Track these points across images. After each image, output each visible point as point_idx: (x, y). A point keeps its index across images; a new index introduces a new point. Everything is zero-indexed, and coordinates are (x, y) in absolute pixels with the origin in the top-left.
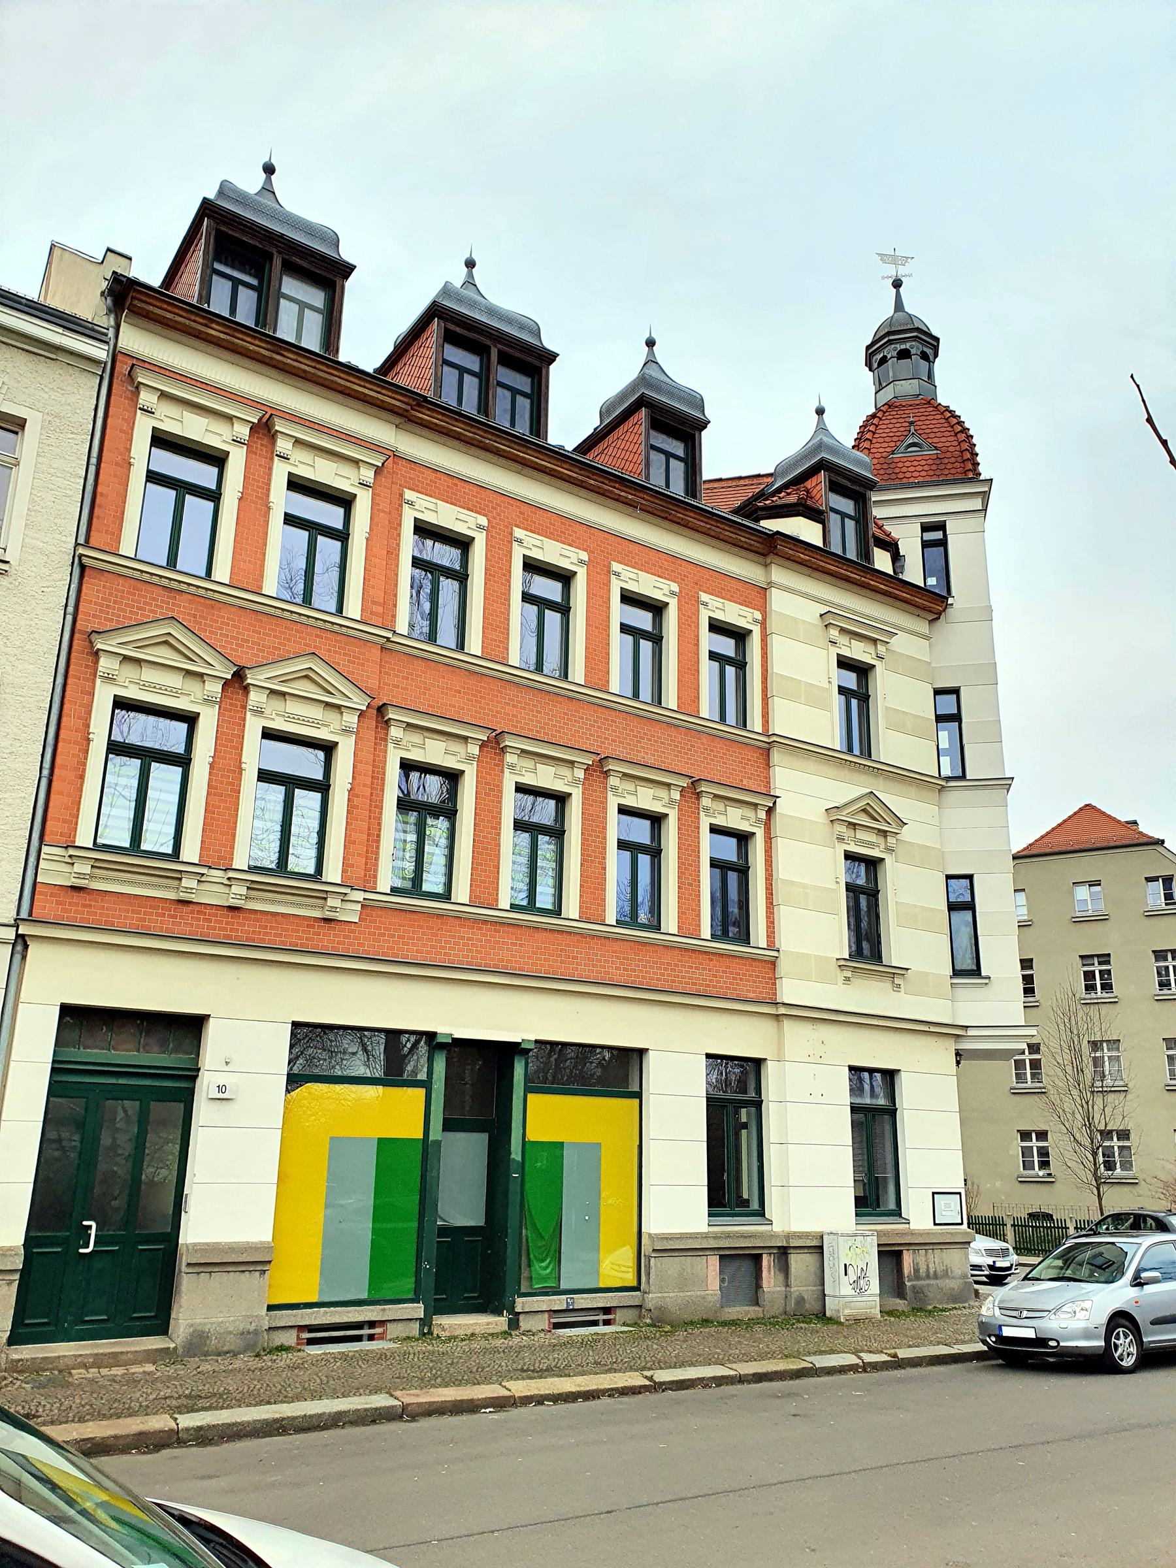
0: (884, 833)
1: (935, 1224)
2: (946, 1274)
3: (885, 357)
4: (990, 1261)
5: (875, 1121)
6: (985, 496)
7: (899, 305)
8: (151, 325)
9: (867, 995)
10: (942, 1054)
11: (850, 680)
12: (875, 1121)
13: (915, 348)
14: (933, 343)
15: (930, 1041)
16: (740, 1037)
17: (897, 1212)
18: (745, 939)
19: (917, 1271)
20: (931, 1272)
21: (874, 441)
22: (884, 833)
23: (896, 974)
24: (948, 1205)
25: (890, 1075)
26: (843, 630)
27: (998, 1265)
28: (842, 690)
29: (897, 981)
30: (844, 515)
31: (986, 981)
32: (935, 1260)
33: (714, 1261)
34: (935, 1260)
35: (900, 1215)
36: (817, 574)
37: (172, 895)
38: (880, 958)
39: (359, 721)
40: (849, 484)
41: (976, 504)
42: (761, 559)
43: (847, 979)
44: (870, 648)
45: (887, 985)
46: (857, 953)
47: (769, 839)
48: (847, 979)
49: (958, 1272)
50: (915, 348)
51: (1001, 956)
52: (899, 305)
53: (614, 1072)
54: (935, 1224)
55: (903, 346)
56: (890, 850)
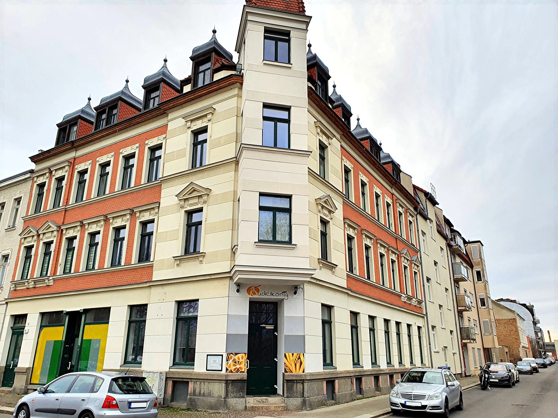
0: (330, 212)
1: (207, 370)
2: (210, 395)
4: (403, 401)
5: (186, 321)
8: (91, 143)
9: (323, 274)
10: (224, 288)
12: (186, 321)
15: (216, 283)
16: (137, 297)
17: (331, 364)
19: (194, 391)
20: (202, 392)
22: (330, 212)
23: (332, 267)
24: (215, 361)
26: (321, 130)
27: (408, 404)
29: (201, 259)
32: (205, 388)
33: (325, 383)
34: (205, 388)
35: (359, 364)
36: (184, 105)
37: (45, 285)
39: (235, 173)
40: (203, 58)
43: (178, 265)
48: (178, 265)
49: (216, 395)
51: (338, 256)
53: (102, 315)
54: (207, 370)
56: (205, 202)
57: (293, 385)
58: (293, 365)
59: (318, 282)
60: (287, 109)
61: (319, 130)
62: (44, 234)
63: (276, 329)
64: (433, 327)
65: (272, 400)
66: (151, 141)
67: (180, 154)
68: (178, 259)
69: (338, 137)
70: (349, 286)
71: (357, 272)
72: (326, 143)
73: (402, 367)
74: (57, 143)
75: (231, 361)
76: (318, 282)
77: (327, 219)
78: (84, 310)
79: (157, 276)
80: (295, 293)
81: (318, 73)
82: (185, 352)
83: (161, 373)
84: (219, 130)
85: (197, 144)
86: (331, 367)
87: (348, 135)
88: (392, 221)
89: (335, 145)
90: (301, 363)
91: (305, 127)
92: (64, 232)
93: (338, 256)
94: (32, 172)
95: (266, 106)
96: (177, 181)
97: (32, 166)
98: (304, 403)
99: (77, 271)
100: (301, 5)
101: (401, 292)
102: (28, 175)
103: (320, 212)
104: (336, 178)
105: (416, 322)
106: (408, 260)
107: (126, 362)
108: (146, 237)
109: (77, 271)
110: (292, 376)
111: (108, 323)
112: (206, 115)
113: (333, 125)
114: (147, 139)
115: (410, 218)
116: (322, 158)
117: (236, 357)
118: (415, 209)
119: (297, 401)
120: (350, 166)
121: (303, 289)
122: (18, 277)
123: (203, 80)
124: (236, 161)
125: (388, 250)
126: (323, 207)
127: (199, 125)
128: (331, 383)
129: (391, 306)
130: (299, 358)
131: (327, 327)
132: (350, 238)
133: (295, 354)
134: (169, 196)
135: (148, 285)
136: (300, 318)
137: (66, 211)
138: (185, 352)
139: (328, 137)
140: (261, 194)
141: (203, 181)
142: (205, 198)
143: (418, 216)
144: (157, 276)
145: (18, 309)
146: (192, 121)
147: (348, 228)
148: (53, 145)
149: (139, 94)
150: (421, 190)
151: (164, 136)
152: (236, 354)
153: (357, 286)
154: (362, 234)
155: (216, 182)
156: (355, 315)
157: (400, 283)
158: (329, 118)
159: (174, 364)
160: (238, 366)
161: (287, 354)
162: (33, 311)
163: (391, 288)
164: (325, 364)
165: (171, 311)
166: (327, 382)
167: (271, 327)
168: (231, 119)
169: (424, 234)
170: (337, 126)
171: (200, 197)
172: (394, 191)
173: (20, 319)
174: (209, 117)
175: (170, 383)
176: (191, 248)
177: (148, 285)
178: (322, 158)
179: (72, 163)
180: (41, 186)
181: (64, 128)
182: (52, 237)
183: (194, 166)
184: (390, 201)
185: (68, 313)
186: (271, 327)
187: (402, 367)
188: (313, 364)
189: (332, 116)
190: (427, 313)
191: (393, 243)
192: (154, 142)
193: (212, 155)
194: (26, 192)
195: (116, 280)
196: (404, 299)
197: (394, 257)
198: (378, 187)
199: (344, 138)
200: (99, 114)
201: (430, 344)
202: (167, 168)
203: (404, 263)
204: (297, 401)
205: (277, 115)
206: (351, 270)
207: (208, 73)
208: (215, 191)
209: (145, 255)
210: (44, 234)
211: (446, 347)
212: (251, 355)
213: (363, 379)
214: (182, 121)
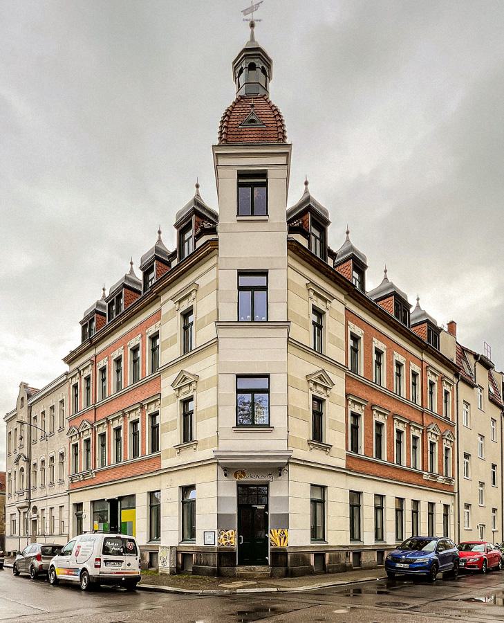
0: (326, 388)
3: (242, 68)
6: (287, 154)
7: (252, 39)
9: (317, 456)
10: (212, 472)
11: (315, 318)
13: (259, 64)
14: (267, 62)
16: (152, 485)
17: (382, 539)
18: (357, 452)
21: (231, 117)
22: (326, 388)
23: (327, 448)
25: (323, 488)
26: (315, 293)
28: (314, 323)
30: (316, 238)
31: (272, 429)
33: (376, 553)
38: (322, 441)
41: (282, 160)
42: (421, 350)
44: (324, 303)
45: (324, 453)
46: (314, 438)
47: (423, 438)
50: (259, 64)
51: (336, 436)
52: (252, 39)
55: (254, 61)
57: (278, 557)
58: (278, 541)
59: (305, 463)
60: (264, 273)
61: (312, 293)
62: (83, 432)
63: (267, 508)
64: (468, 506)
65: (260, 569)
66: (150, 329)
67: (172, 341)
68: (179, 449)
69: (342, 298)
70: (350, 465)
71: (362, 451)
72: (323, 309)
73: (358, 544)
74: (83, 341)
75: (222, 537)
76: (305, 463)
77: (322, 396)
78: (119, 497)
79: (165, 463)
80: (280, 475)
81: (308, 219)
82: (189, 529)
83: (171, 547)
84: (204, 307)
85: (186, 327)
86: (323, 542)
87: (355, 295)
88: (419, 393)
89: (337, 307)
90: (285, 538)
91: (291, 289)
92: (97, 429)
93: (336, 436)
94: (67, 374)
95: (241, 273)
96: (171, 370)
97: (66, 368)
98: (287, 571)
99: (109, 464)
100: (278, 118)
101: (423, 470)
102: (65, 378)
103: (311, 389)
104: (336, 350)
105: (440, 500)
106: (436, 435)
107: (151, 540)
108: (155, 429)
109: (109, 464)
110: (277, 549)
111: (135, 508)
112: (190, 294)
113: (333, 284)
114: (147, 328)
115: (447, 388)
116: (319, 326)
117: (227, 533)
118: (456, 375)
119: (282, 570)
120: (358, 331)
121: (288, 471)
122: (72, 472)
123: (189, 249)
124: (216, 342)
125: (409, 425)
126: (315, 384)
127: (185, 305)
128: (357, 554)
129: (408, 484)
130: (284, 533)
131: (319, 507)
132: (356, 416)
133: (280, 530)
134: (166, 387)
135: (158, 473)
136: (290, 499)
137: (95, 409)
138: (189, 529)
139: (326, 301)
140: (238, 376)
141: (191, 368)
142: (194, 385)
143: (461, 384)
144: (165, 463)
145: (76, 498)
146: (180, 302)
147: (352, 405)
148: (80, 343)
149: (139, 275)
150: (470, 352)
151: (159, 322)
152: (227, 531)
153: (355, 466)
154: (373, 410)
155: (203, 367)
156: (356, 496)
157: (423, 461)
158: (327, 276)
159: (183, 541)
160: (229, 541)
161: (272, 531)
162: (86, 498)
163: (408, 466)
164: (352, 538)
165: (176, 495)
166: (315, 555)
167: (262, 507)
168: (213, 290)
169: (468, 404)
170: (339, 285)
171: (190, 384)
172: (425, 358)
173: (79, 506)
174: (193, 294)
175: (180, 556)
176: (187, 436)
177: (158, 473)
178: (319, 326)
179: (94, 363)
180: (76, 387)
181: (87, 324)
182: (88, 435)
183: (185, 351)
184: (417, 369)
185: (109, 501)
186: (262, 507)
187: (358, 544)
188: (297, 537)
189: (331, 274)
190: (458, 491)
191: (418, 418)
192: (152, 331)
193: (200, 336)
194: (66, 393)
195: (137, 470)
196: (426, 476)
197: (417, 433)
198: (403, 353)
199: (349, 298)
200: (111, 305)
201: (459, 522)
202: (165, 357)
203: (431, 438)
204: (282, 570)
205: (253, 282)
206: (355, 448)
207: (192, 241)
208: (204, 376)
209: (155, 446)
210: (83, 432)
211: (484, 525)
212: (241, 530)
213: (363, 553)
214: (171, 304)
